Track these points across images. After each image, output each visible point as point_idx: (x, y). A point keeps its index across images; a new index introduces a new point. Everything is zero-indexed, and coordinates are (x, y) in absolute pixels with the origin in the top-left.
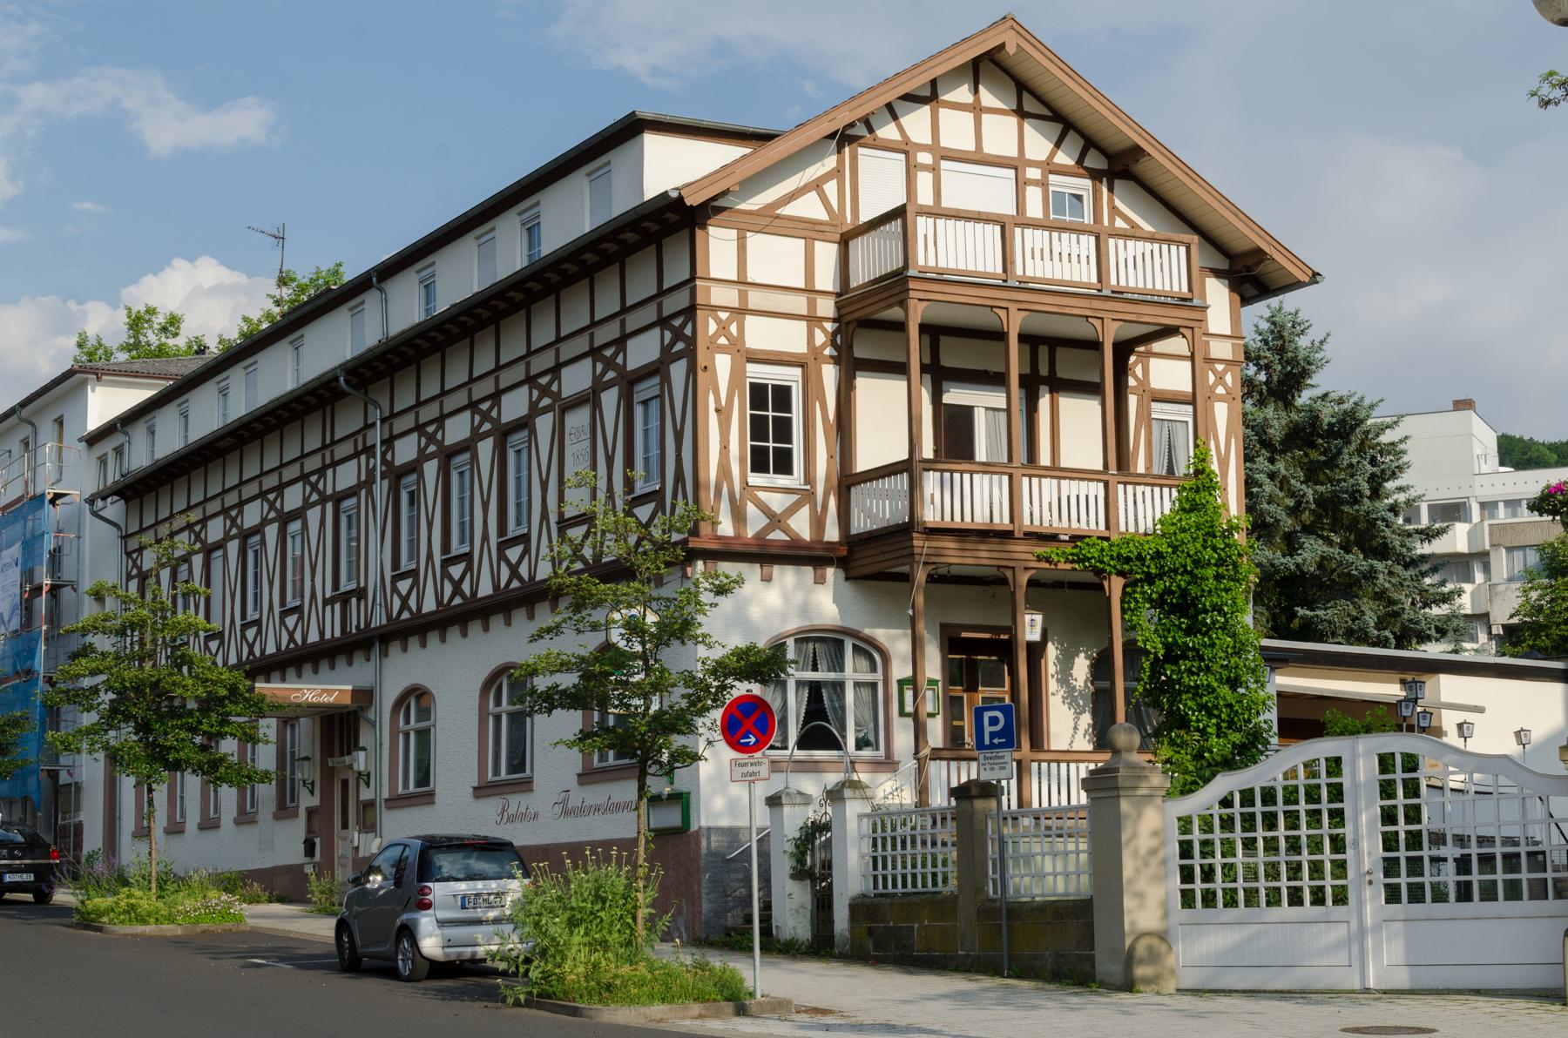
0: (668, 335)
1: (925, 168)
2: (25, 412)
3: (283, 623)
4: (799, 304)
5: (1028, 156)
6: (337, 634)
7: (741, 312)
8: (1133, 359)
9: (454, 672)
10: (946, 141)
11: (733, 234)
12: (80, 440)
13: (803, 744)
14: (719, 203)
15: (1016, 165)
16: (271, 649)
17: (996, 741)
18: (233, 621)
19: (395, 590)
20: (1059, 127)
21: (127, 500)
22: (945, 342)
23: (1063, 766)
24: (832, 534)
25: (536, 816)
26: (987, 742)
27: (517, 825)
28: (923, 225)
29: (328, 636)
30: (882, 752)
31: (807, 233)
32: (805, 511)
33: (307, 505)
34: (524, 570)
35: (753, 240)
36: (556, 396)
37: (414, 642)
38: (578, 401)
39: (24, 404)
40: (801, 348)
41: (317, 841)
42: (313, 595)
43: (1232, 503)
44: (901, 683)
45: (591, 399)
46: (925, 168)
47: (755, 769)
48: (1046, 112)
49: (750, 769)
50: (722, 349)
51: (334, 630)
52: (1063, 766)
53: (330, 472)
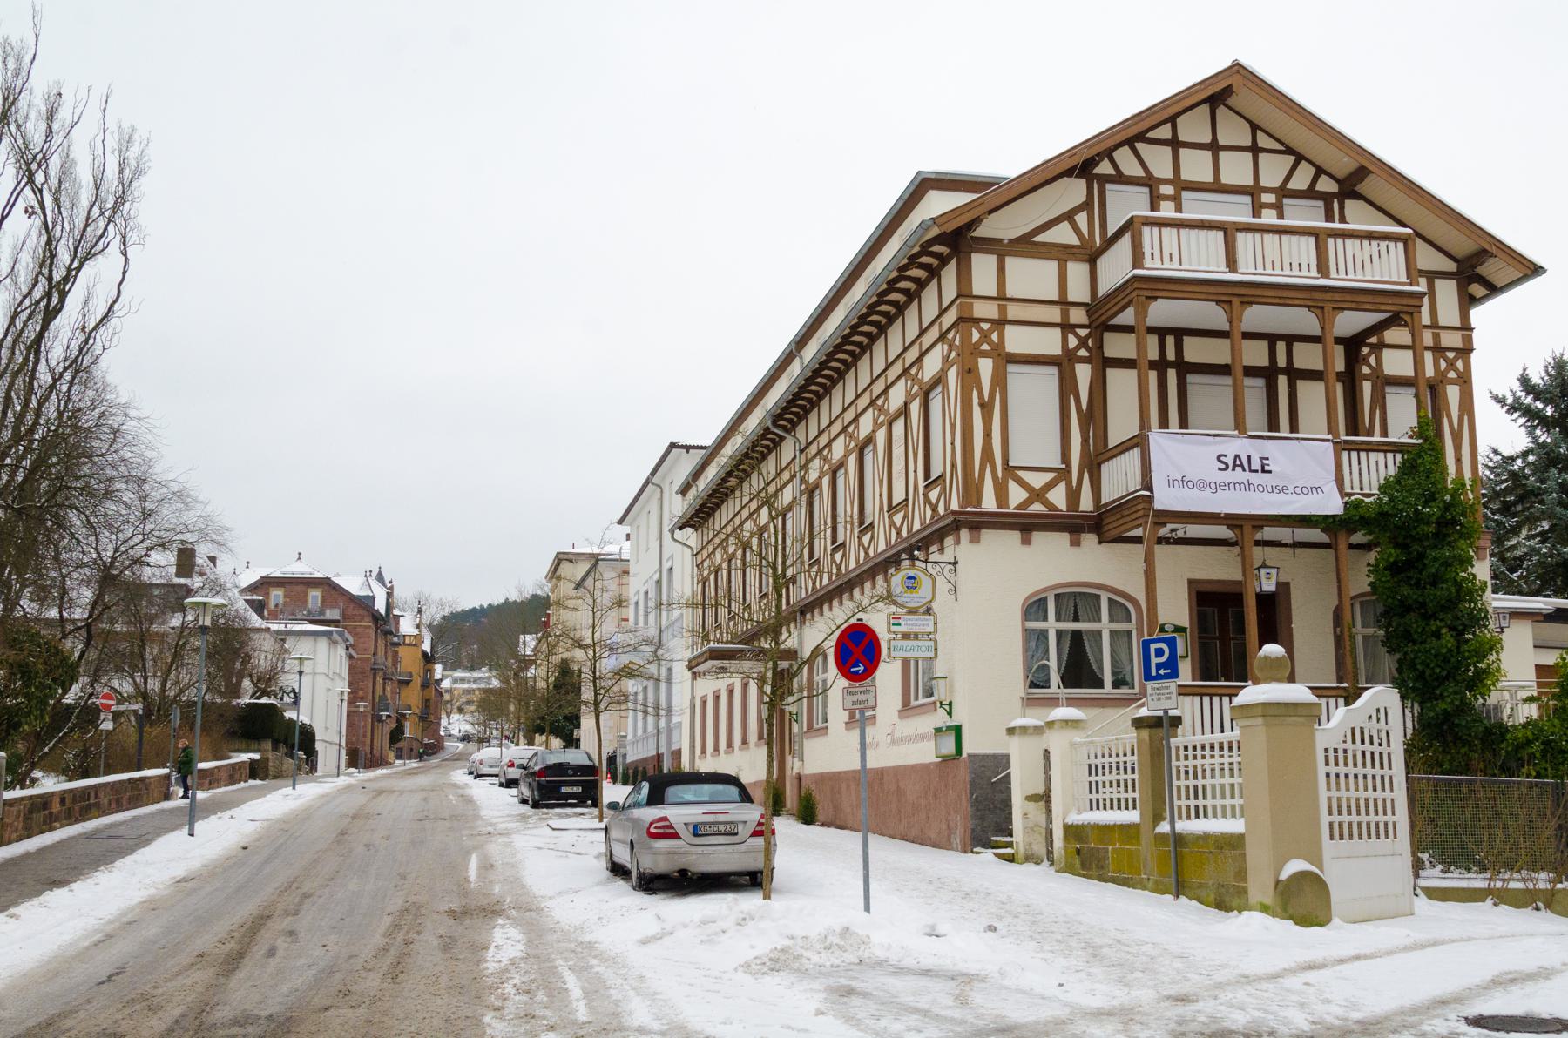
1: (1167, 198)
2: (655, 480)
4: (1054, 314)
7: (1001, 323)
8: (1365, 350)
10: (1187, 175)
11: (994, 258)
14: (980, 232)
15: (1253, 192)
17: (1162, 672)
30: (1137, 690)
32: (1062, 487)
35: (1010, 262)
39: (653, 473)
40: (1056, 350)
45: (905, 411)
46: (1167, 198)
47: (864, 697)
50: (985, 354)
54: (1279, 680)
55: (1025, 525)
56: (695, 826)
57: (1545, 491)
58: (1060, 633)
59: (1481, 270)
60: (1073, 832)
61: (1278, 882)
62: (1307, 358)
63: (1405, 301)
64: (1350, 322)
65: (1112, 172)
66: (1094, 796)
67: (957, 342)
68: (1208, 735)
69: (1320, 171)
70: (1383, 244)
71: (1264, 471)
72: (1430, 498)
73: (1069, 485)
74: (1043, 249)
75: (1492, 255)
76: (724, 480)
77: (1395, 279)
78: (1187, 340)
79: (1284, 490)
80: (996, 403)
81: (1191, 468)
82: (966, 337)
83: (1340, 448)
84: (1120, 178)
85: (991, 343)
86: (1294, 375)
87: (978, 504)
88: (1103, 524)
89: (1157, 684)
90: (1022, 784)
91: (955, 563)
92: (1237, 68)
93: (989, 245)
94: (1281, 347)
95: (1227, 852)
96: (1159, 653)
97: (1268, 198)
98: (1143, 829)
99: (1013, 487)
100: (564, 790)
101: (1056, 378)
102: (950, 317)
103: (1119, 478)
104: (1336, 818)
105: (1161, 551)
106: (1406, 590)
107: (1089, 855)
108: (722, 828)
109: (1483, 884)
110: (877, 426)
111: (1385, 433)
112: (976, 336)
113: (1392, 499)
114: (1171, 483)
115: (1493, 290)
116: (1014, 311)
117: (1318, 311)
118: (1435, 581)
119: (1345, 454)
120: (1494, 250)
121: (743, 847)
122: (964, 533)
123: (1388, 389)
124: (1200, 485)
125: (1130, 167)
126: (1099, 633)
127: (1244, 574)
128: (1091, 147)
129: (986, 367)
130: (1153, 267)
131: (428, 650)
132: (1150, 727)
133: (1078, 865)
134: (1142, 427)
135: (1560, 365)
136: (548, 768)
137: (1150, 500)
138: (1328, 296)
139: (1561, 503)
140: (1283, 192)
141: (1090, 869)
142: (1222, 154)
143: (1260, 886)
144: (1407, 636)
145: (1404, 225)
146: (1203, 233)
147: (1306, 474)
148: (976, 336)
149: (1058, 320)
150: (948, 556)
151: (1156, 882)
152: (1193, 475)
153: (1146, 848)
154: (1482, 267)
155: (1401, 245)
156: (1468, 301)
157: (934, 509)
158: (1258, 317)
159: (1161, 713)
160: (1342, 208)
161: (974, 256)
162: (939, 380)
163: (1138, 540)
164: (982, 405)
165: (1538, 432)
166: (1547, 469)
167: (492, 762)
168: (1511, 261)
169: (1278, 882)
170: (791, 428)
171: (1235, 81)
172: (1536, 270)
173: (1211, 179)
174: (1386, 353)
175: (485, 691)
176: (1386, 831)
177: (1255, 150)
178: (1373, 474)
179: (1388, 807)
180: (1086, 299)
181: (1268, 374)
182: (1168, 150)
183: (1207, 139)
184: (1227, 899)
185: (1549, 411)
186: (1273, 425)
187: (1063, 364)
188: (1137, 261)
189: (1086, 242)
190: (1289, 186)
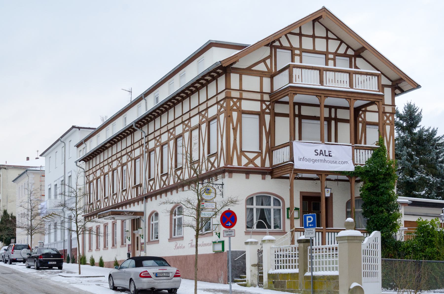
0: (219, 107)
1: (297, 55)
2: (62, 140)
4: (258, 96)
7: (240, 99)
8: (361, 112)
9: (160, 206)
10: (304, 47)
12: (75, 146)
14: (234, 66)
15: (326, 54)
16: (119, 201)
18: (110, 194)
19: (149, 184)
20: (339, 42)
21: (86, 162)
22: (303, 107)
23: (330, 233)
24: (267, 165)
25: (184, 247)
26: (308, 226)
27: (179, 249)
28: (296, 72)
29: (133, 197)
30: (282, 229)
31: (261, 75)
34: (181, 177)
35: (244, 77)
36: (190, 127)
37: (154, 198)
38: (195, 128)
39: (62, 137)
40: (258, 110)
41: (131, 253)
42: (129, 187)
46: (297, 55)
47: (230, 233)
48: (336, 38)
49: (229, 233)
50: (235, 110)
51: (134, 196)
53: (133, 152)
54: (352, 229)
55: (247, 172)
56: (156, 274)
58: (257, 209)
59: (400, 85)
60: (270, 276)
61: (349, 289)
62: (342, 114)
63: (377, 97)
64: (358, 103)
65: (279, 44)
66: (277, 265)
67: (225, 105)
68: (333, 245)
69: (348, 47)
70: (368, 76)
71: (329, 156)
72: (383, 166)
73: (262, 158)
75: (404, 81)
76: (106, 144)
79: (336, 162)
80: (238, 128)
81: (308, 154)
82: (228, 104)
84: (281, 47)
85: (237, 106)
86: (337, 120)
87: (232, 164)
88: (273, 172)
89: (308, 229)
90: (251, 260)
91: (223, 185)
92: (324, 9)
93: (237, 71)
94: (333, 110)
95: (331, 281)
96: (310, 219)
97: (331, 56)
98: (299, 275)
100: (49, 263)
101: (258, 119)
102: (222, 96)
103: (280, 157)
106: (373, 197)
108: (165, 274)
110: (184, 131)
111: (365, 143)
112: (232, 103)
114: (300, 159)
115: (403, 92)
116: (245, 95)
117: (349, 100)
118: (382, 194)
119: (355, 150)
120: (405, 79)
121: (171, 280)
122: (227, 174)
123: (367, 126)
124: (309, 160)
125: (285, 43)
126: (270, 209)
128: (275, 36)
129: (235, 115)
130: (297, 83)
132: (304, 243)
134: (291, 140)
136: (43, 255)
137: (293, 165)
138: (353, 95)
139: (407, 160)
140: (336, 54)
141: (278, 288)
142: (316, 39)
144: (372, 213)
145: (378, 70)
146: (313, 71)
147: (342, 157)
148: (232, 103)
150: (219, 182)
153: (300, 280)
155: (376, 77)
156: (394, 95)
157: (213, 164)
158: (330, 101)
159: (309, 238)
160: (355, 61)
161: (231, 74)
163: (288, 178)
164: (233, 129)
165: (400, 132)
166: (403, 147)
169: (349, 289)
171: (323, 14)
172: (418, 86)
176: (375, 274)
177: (327, 38)
178: (364, 157)
179: (376, 267)
180: (269, 91)
181: (328, 120)
182: (298, 37)
183: (311, 34)
185: (405, 124)
186: (329, 140)
187: (261, 114)
188: (291, 81)
189: (269, 70)
190: (338, 52)
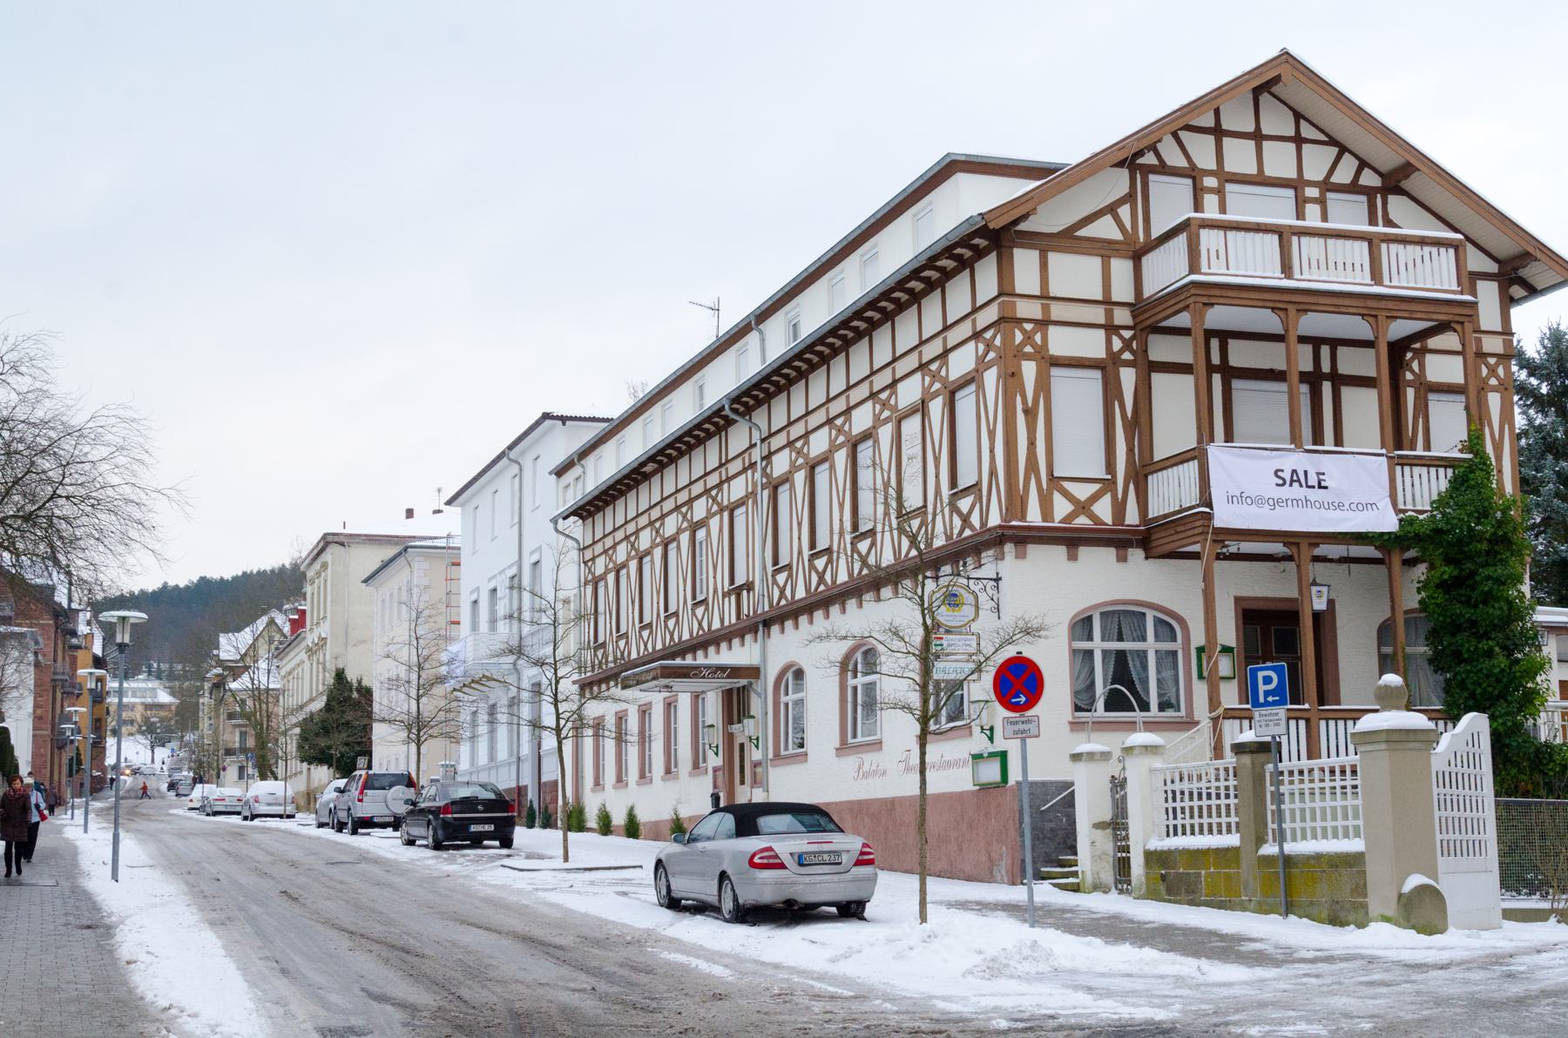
0: (981, 347)
1: (1211, 190)
2: (512, 454)
3: (694, 614)
4: (1098, 314)
5: (1307, 177)
6: (734, 620)
7: (1044, 323)
8: (1409, 355)
9: (809, 648)
10: (1231, 166)
11: (1036, 253)
13: (1109, 707)
14: (1022, 227)
15: (1296, 185)
17: (1270, 699)
19: (775, 582)
20: (1335, 150)
21: (583, 518)
25: (884, 772)
26: (1262, 700)
30: (1183, 712)
32: (1107, 498)
33: (710, 515)
34: (872, 560)
35: (1053, 257)
36: (894, 409)
39: (510, 448)
40: (1101, 354)
41: (721, 795)
42: (715, 591)
43: (1507, 480)
44: (1200, 650)
45: (922, 408)
46: (1211, 190)
47: (1025, 727)
48: (1323, 138)
49: (1021, 727)
50: (1028, 357)
52: (1332, 723)
53: (725, 486)
54: (1398, 708)
55: (1072, 540)
56: (800, 857)
57: (1542, 482)
58: (1105, 653)
59: (1524, 273)
60: (1153, 858)
61: (1400, 895)
62: (1353, 362)
64: (1401, 328)
67: (998, 342)
68: (1334, 758)
69: (1363, 164)
70: (1427, 249)
71: (1320, 487)
73: (1114, 497)
74: (1087, 245)
75: (1536, 259)
76: (643, 464)
77: (1446, 287)
78: (1232, 343)
79: (1340, 506)
80: (1039, 409)
81: (1254, 483)
83: (1397, 462)
84: (1163, 169)
86: (1339, 380)
87: (1023, 518)
88: (1150, 539)
89: (1265, 711)
90: (1089, 810)
91: (997, 580)
94: (1325, 351)
95: (1343, 871)
96: (1268, 680)
97: (1312, 192)
98: (1243, 854)
99: (1058, 498)
100: (474, 828)
102: (991, 314)
103: (1171, 493)
104: (1445, 837)
105: (1220, 567)
106: (1458, 609)
107: (1174, 877)
108: (826, 857)
109: (1545, 905)
111: (1427, 447)
112: (1019, 337)
113: (1444, 514)
114: (1230, 499)
115: (1533, 291)
116: (1058, 311)
118: (1487, 598)
120: (1539, 255)
124: (1258, 501)
125: (1175, 159)
127: (1301, 593)
128: (1139, 140)
129: (1029, 370)
130: (1213, 271)
131: (100, 653)
132: (1251, 752)
133: (1162, 889)
134: (1200, 441)
135: (1556, 336)
136: (454, 803)
138: (1382, 304)
139: (1557, 495)
140: (1327, 186)
143: (1380, 898)
144: (1457, 657)
145: (1456, 230)
147: (1362, 491)
148: (1019, 337)
149: (1102, 321)
150: (988, 570)
151: (1259, 903)
152: (1252, 491)
153: (1246, 871)
154: (1520, 268)
155: (1451, 251)
156: (1508, 301)
157: (966, 520)
158: (1314, 323)
159: (1269, 739)
160: (1385, 204)
162: (973, 379)
163: (1195, 556)
164: (1026, 412)
165: (1532, 412)
166: (1543, 456)
167: (271, 799)
168: (1552, 264)
169: (1400, 895)
170: (748, 411)
171: (1284, 71)
173: (1255, 172)
174: (1429, 358)
175: (148, 707)
176: (1476, 848)
177: (1298, 140)
178: (1426, 490)
179: (1480, 825)
180: (1130, 298)
181: (1313, 379)
182: (1211, 139)
183: (1251, 128)
184: (1342, 915)
185: (1544, 390)
186: (1318, 438)
187: (1107, 368)
188: (1194, 267)
189: (1129, 237)
190: (1333, 180)
